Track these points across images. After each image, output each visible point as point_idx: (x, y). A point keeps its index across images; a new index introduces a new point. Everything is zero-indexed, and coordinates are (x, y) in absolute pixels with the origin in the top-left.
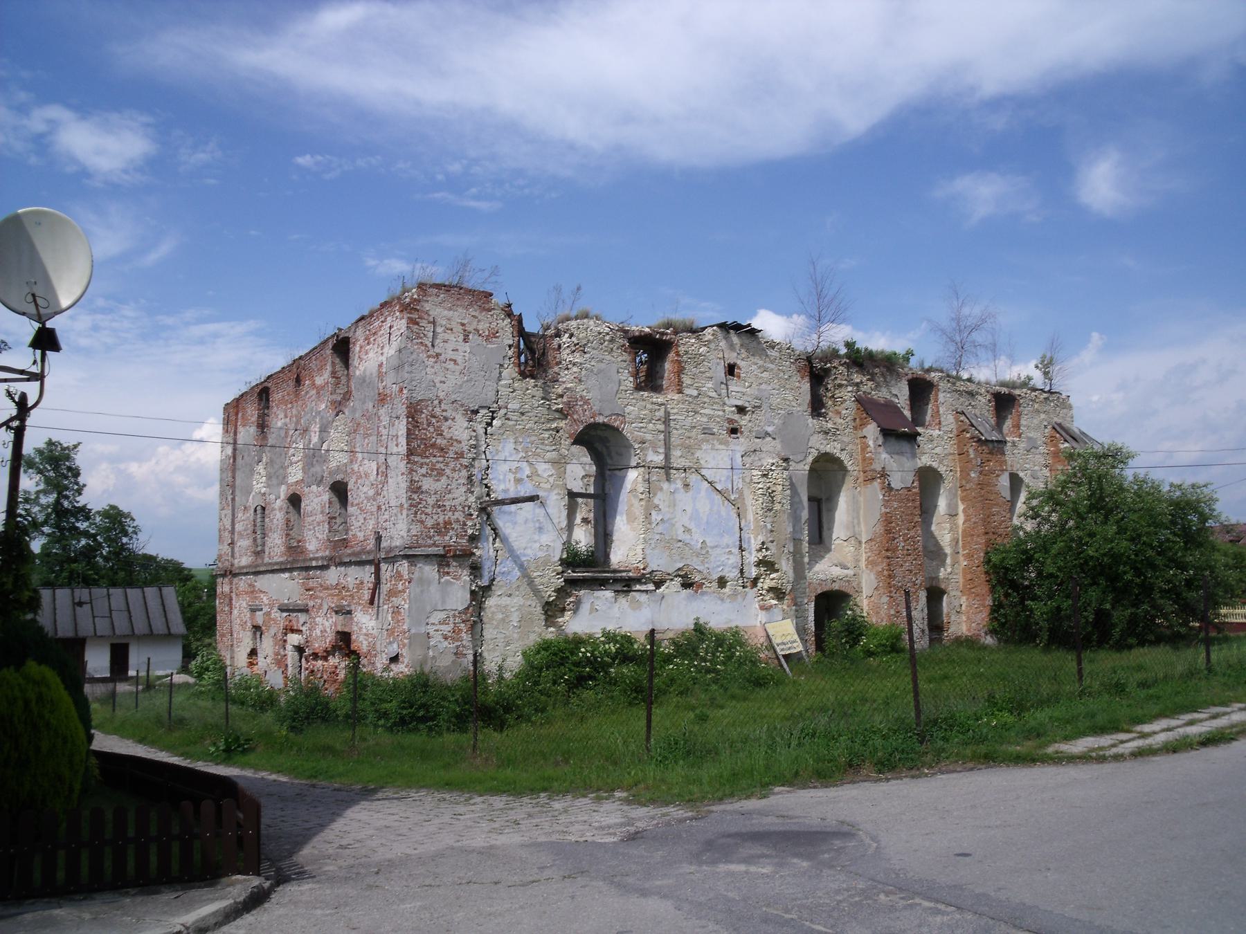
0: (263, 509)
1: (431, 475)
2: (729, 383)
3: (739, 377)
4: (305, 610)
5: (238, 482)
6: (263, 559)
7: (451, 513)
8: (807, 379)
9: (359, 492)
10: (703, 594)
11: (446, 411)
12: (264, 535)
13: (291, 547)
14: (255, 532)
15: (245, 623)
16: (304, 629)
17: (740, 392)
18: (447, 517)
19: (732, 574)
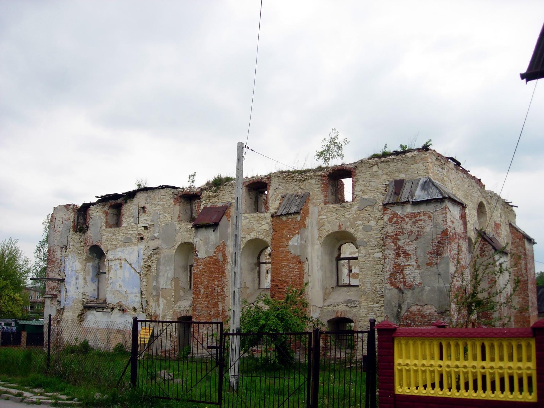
10: (126, 314)
17: (145, 220)
19: (138, 306)
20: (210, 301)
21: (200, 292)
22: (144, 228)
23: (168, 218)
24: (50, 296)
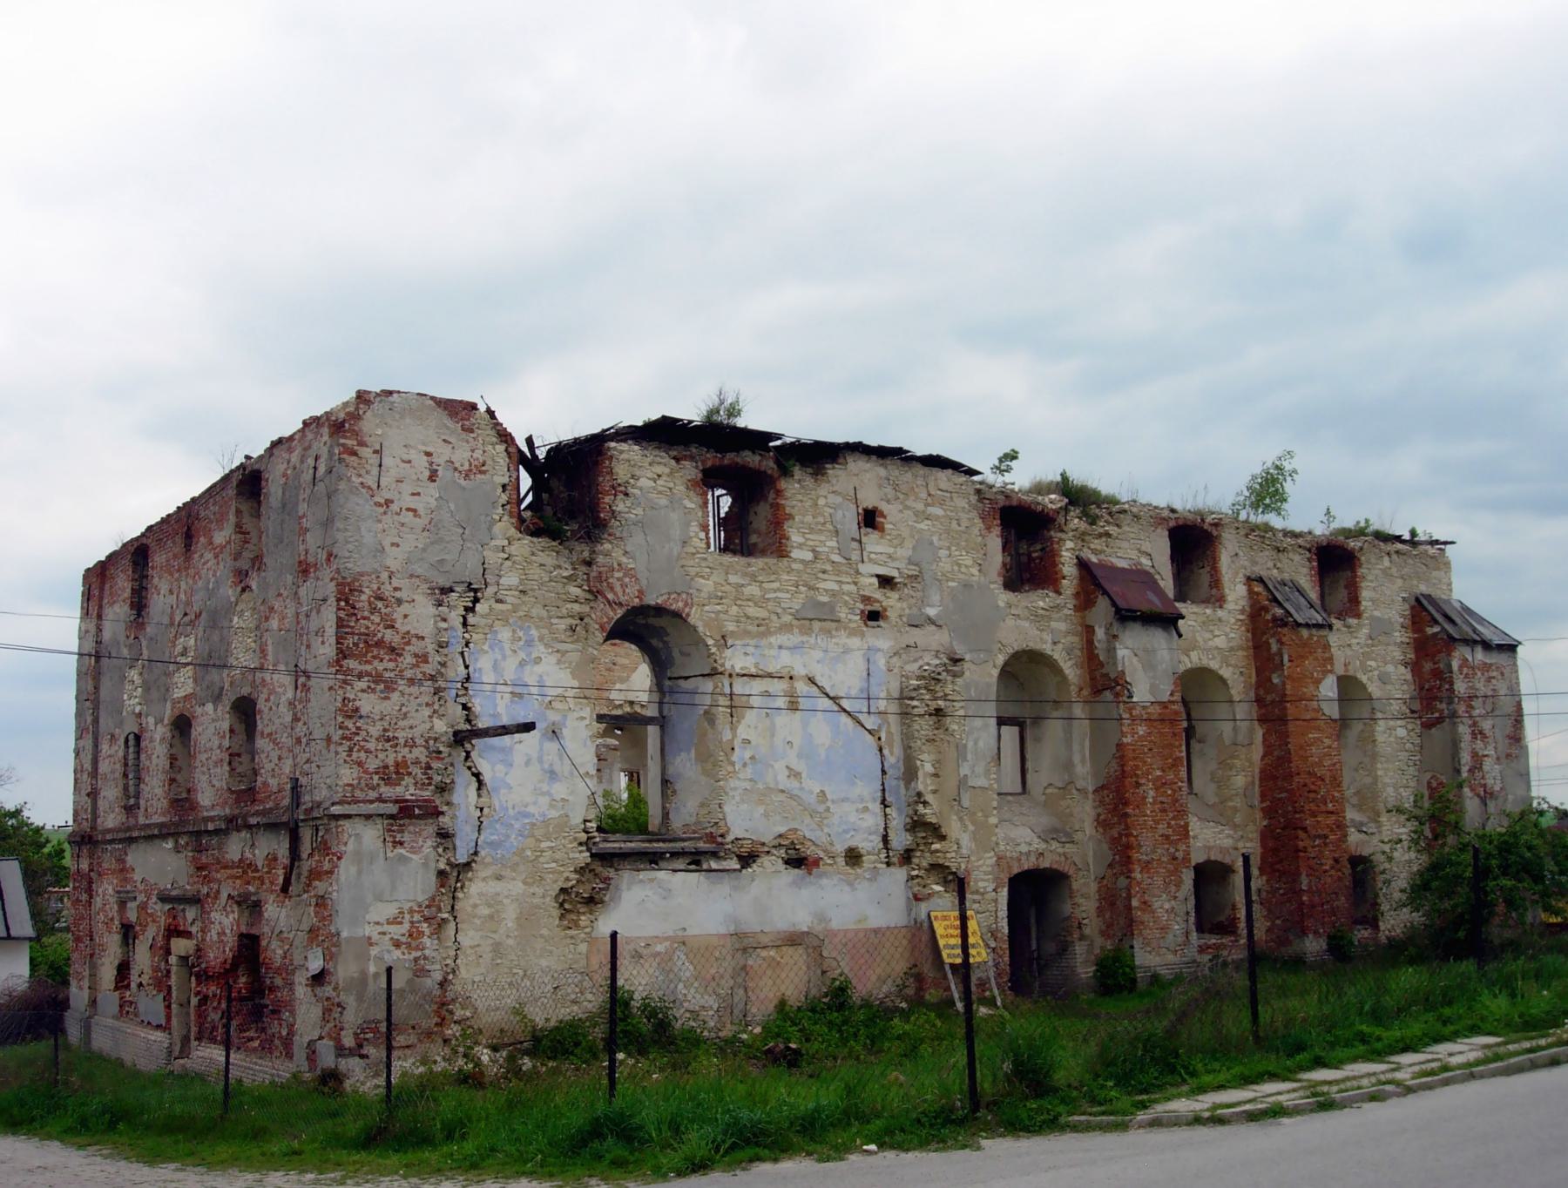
0: (138, 738)
1: (374, 691)
2: (864, 539)
3: (882, 530)
4: (195, 900)
5: (103, 693)
6: (136, 818)
7: (407, 749)
8: (997, 531)
9: (274, 715)
10: (820, 876)
11: (400, 589)
12: (139, 779)
13: (178, 800)
14: (125, 775)
15: (112, 919)
16: (194, 929)
17: (880, 552)
18: (400, 755)
19: (868, 843)
20: (1173, 822)
21: (1144, 798)
22: (879, 583)
23: (966, 566)
24: (392, 809)
